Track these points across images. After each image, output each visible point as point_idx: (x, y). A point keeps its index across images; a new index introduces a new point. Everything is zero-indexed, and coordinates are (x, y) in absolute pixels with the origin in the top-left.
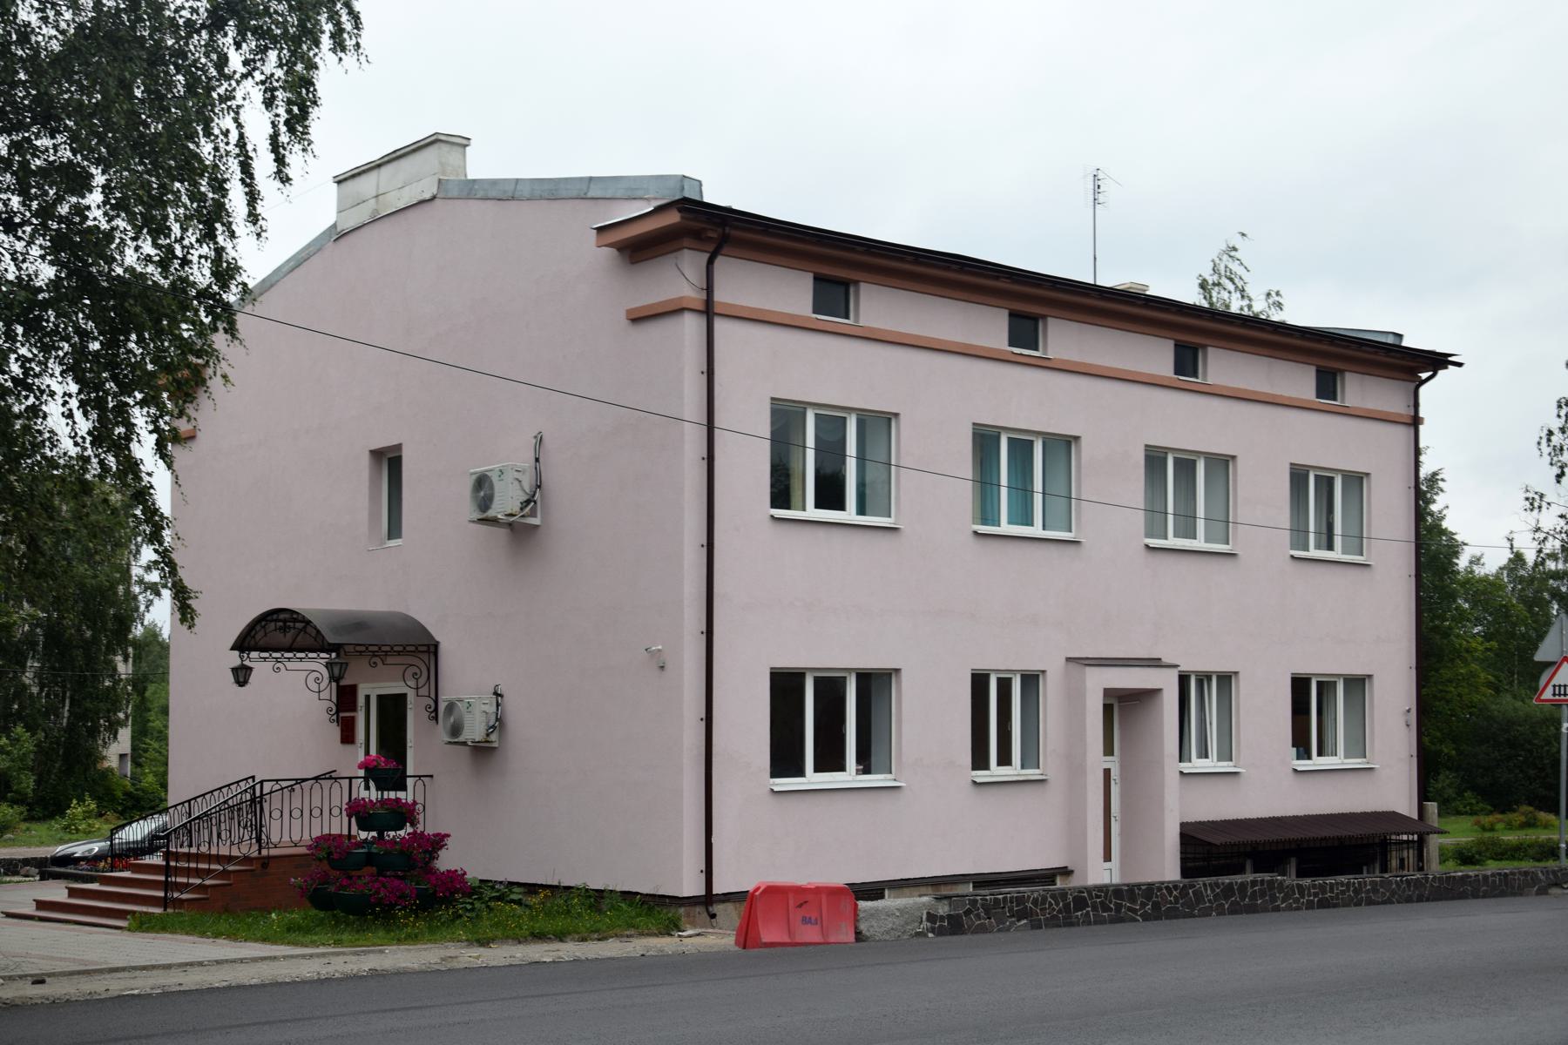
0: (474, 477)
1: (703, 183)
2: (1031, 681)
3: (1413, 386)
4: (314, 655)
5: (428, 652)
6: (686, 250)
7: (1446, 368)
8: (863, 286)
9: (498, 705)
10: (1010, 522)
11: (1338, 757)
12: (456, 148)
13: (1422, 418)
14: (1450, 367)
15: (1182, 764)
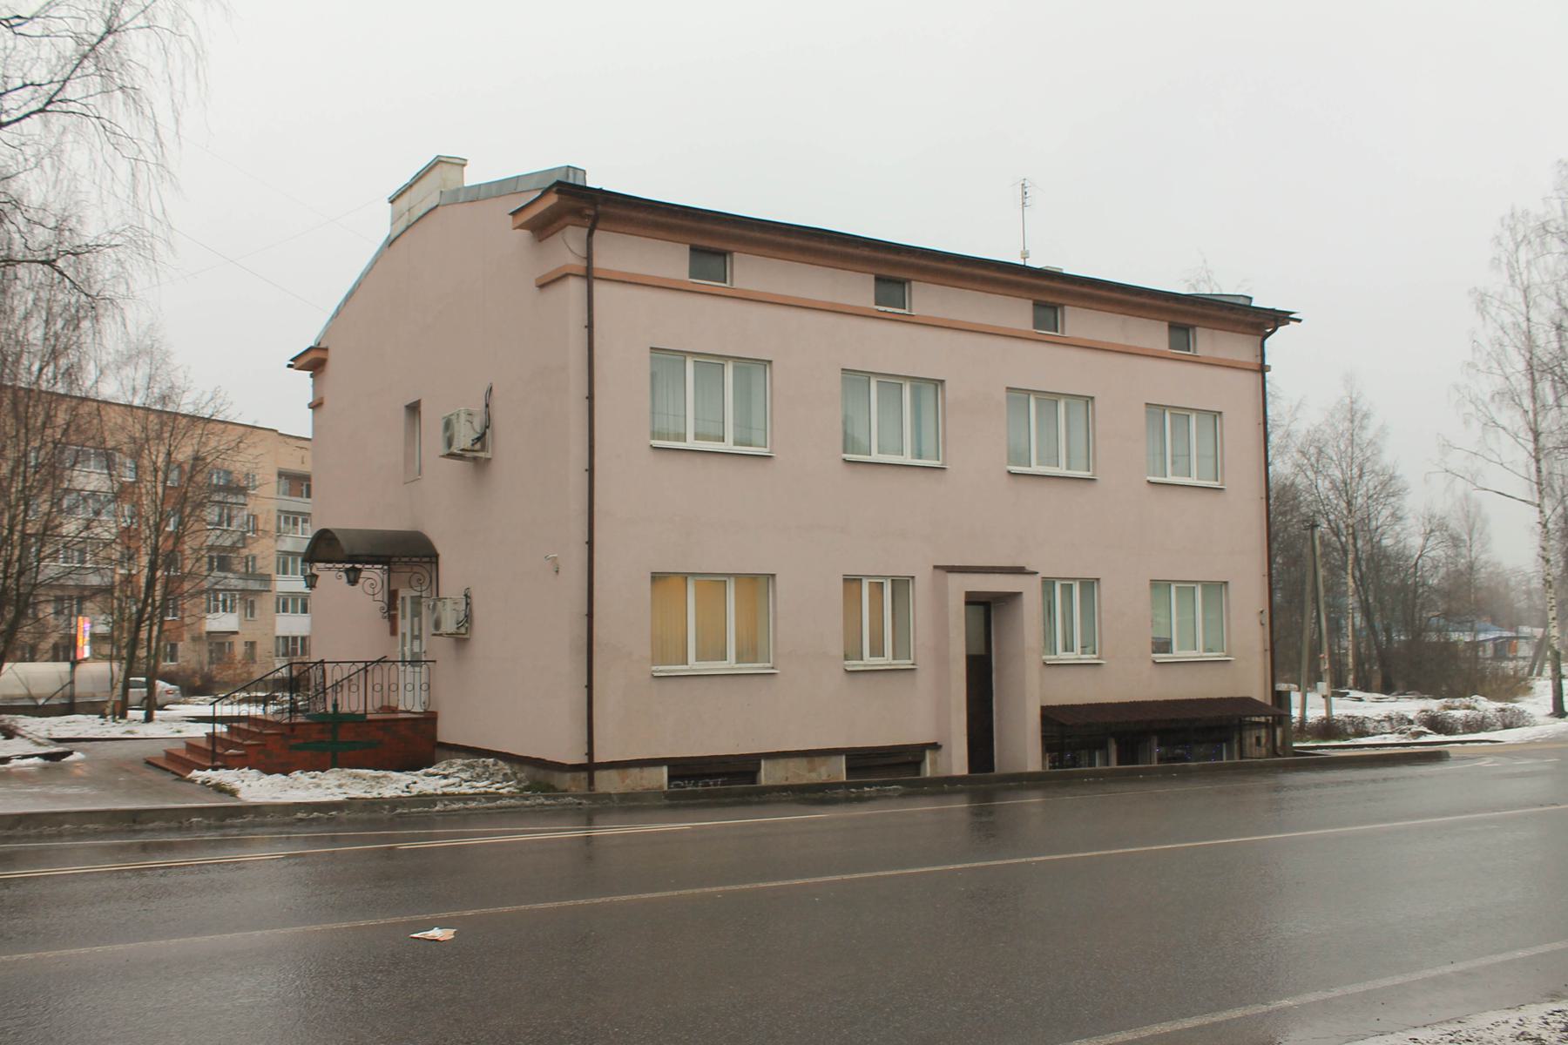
0: (445, 420)
1: (587, 172)
2: (901, 585)
3: (1259, 338)
4: (370, 566)
5: (431, 562)
6: (570, 227)
7: (1288, 323)
8: (736, 255)
9: (467, 604)
10: (1039, 464)
11: (1074, 653)
12: (457, 167)
13: (1269, 366)
14: (1291, 323)
15: (846, 663)
